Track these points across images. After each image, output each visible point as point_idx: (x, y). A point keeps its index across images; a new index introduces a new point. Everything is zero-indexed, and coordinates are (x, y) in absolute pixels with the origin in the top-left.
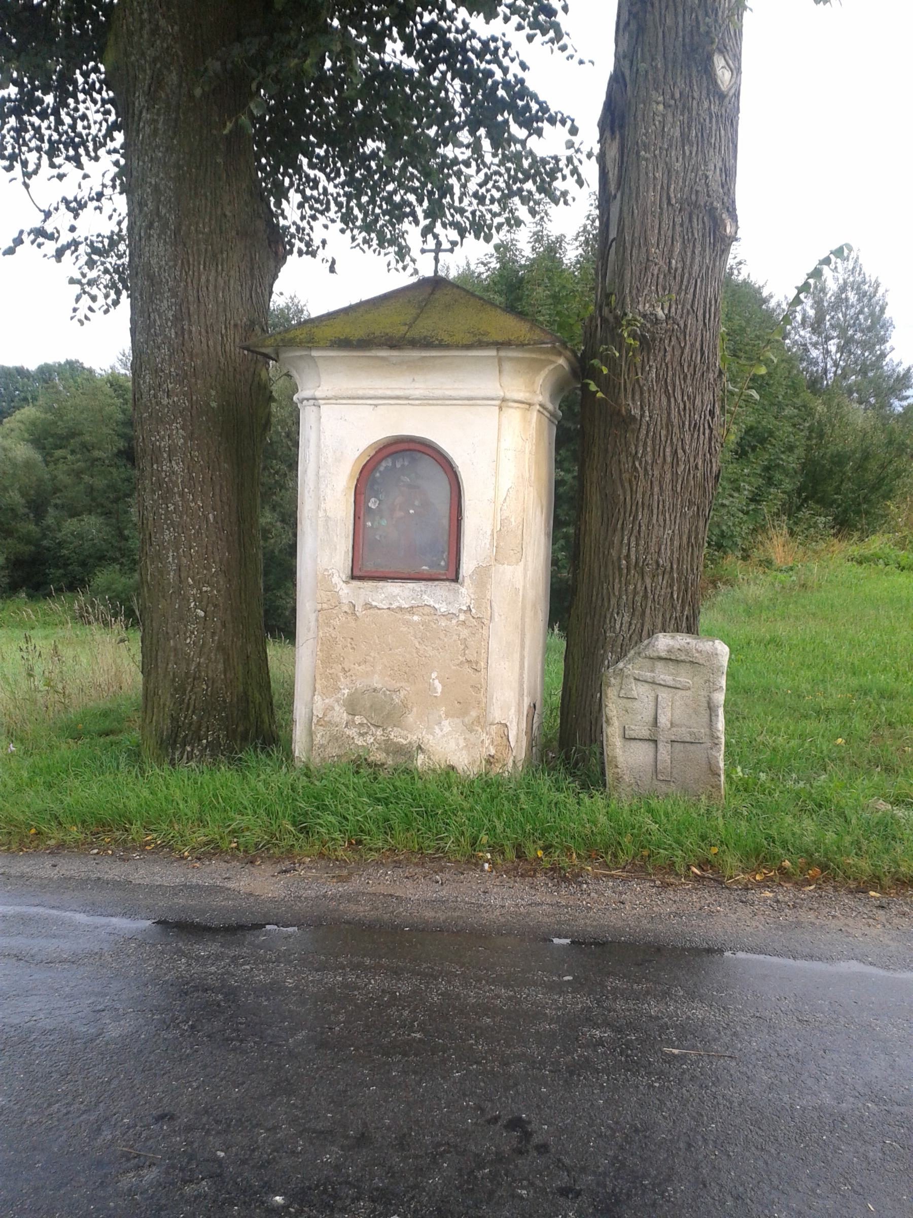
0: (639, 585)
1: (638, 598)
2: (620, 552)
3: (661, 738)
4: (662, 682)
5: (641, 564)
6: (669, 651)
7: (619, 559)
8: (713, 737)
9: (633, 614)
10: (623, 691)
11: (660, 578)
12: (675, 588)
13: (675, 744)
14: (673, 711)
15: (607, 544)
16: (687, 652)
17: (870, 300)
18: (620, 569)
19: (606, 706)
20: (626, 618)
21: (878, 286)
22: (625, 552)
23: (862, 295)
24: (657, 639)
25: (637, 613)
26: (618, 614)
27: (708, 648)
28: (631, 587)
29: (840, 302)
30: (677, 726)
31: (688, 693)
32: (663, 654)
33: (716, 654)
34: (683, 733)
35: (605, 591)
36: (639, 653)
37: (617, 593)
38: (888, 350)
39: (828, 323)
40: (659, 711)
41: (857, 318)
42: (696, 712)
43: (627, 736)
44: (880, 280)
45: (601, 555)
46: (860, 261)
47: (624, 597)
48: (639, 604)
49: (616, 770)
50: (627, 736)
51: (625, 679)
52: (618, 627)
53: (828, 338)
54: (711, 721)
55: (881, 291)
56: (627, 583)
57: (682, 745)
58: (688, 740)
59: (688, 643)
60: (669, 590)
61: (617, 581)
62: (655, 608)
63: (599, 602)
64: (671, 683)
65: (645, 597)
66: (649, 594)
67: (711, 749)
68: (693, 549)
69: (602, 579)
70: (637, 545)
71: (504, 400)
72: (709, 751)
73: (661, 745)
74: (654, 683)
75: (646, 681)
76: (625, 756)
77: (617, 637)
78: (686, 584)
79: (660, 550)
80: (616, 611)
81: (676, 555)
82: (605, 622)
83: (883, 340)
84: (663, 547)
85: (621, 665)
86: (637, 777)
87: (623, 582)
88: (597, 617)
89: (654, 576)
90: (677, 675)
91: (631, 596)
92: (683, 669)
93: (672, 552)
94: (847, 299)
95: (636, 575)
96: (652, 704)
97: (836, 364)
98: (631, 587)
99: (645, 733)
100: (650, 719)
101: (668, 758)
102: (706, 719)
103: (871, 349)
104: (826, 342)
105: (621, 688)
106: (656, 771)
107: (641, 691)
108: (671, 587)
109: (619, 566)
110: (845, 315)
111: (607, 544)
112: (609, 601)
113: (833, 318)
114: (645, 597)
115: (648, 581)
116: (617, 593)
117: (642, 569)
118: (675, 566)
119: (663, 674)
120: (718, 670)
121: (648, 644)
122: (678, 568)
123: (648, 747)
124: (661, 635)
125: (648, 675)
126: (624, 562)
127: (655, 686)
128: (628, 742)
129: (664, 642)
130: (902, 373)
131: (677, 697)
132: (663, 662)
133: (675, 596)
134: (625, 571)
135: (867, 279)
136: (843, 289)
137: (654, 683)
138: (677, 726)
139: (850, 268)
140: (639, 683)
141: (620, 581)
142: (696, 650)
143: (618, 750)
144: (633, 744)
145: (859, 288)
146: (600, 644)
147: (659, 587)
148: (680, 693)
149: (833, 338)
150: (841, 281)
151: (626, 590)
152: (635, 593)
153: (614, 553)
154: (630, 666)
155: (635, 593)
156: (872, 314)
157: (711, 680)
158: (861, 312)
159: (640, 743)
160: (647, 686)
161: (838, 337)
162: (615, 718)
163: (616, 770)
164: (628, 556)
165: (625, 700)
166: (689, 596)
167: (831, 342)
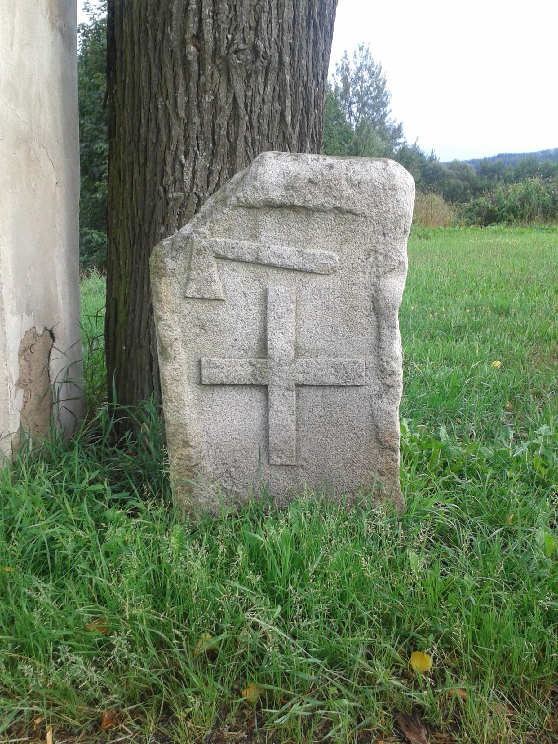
0: (222, 93)
1: (222, 120)
2: (184, 30)
3: (277, 381)
4: (275, 261)
5: (223, 50)
6: (289, 187)
7: (183, 43)
8: (382, 372)
9: (214, 154)
10: (192, 285)
11: (261, 79)
12: (288, 102)
13: (305, 391)
14: (300, 321)
15: (159, 19)
16: (328, 186)
17: (376, 78)
18: (186, 63)
19: (160, 318)
20: (202, 162)
21: (381, 68)
22: (192, 28)
23: (371, 74)
24: (261, 164)
25: (221, 151)
26: (186, 155)
27: (375, 175)
28: (208, 99)
29: (358, 79)
30: (309, 353)
31: (330, 281)
32: (276, 195)
33: (393, 188)
34: (321, 368)
35: (161, 112)
36: (224, 201)
37: (182, 114)
38: (388, 111)
39: (351, 93)
40: (271, 324)
41: (369, 90)
42: (347, 321)
43: (206, 381)
44: (382, 65)
45: (150, 44)
46: (370, 51)
47: (196, 120)
48: (223, 132)
49: (185, 452)
50: (206, 381)
51: (196, 259)
52: (187, 178)
53: (351, 103)
54: (379, 339)
55: (383, 71)
56: (201, 91)
57: (319, 392)
58: (332, 380)
59: (331, 167)
60: (277, 106)
61: (181, 89)
62: (253, 140)
63: (153, 137)
64: (295, 261)
65: (235, 116)
66: (242, 112)
67: (379, 396)
68: (316, 34)
69: (155, 89)
70: (216, 13)
71: (264, 388)
72: (376, 403)
73: (275, 396)
74: (257, 263)
75: (240, 261)
76: (205, 422)
77: (187, 198)
78: (306, 99)
79: (258, 22)
80: (182, 148)
81: (287, 38)
82: (163, 172)
83: (385, 105)
84: (264, 18)
85: (187, 229)
86: (229, 461)
87: (193, 90)
88: (150, 164)
89: (249, 76)
90: (309, 241)
91: (208, 117)
92: (321, 227)
93: (281, 29)
94: (363, 76)
95: (217, 75)
96: (256, 309)
97: (356, 120)
98: (208, 99)
99: (242, 371)
100: (254, 342)
101: (290, 421)
102: (367, 337)
103: (378, 111)
104: (350, 106)
105: (188, 279)
106: (267, 448)
107: (230, 282)
108: (281, 100)
109: (185, 57)
110: (361, 87)
111: (159, 19)
112: (170, 130)
113: (354, 89)
114: (235, 116)
115: (238, 85)
116: (182, 114)
117: (226, 60)
118: (287, 59)
119: (277, 241)
120: (396, 224)
121: (242, 179)
122: (291, 66)
123: (250, 401)
124: (269, 154)
125: (246, 246)
126: (192, 48)
127: (259, 270)
128: (209, 393)
129: (275, 169)
130: (397, 126)
131: (307, 292)
132: (275, 215)
133: (289, 119)
134: (195, 67)
135: (375, 64)
136: (360, 69)
137: (257, 263)
138: (309, 353)
139: (364, 55)
140: (227, 267)
141: (187, 91)
142: (349, 180)
143: (187, 410)
144: (219, 395)
145: (369, 70)
146: (158, 215)
147: (258, 99)
148: (314, 282)
149: (354, 103)
150: (359, 65)
151: (199, 106)
152: (216, 108)
153: (174, 36)
154: (204, 229)
155: (216, 108)
156: (378, 87)
157: (380, 248)
158: (371, 86)
159: (232, 395)
160: (243, 271)
161: (358, 102)
162: (178, 345)
163: (185, 452)
164: (198, 37)
165: (199, 305)
166: (312, 123)
167: (353, 106)
